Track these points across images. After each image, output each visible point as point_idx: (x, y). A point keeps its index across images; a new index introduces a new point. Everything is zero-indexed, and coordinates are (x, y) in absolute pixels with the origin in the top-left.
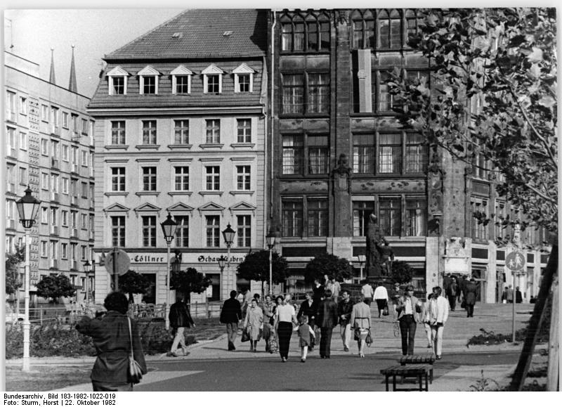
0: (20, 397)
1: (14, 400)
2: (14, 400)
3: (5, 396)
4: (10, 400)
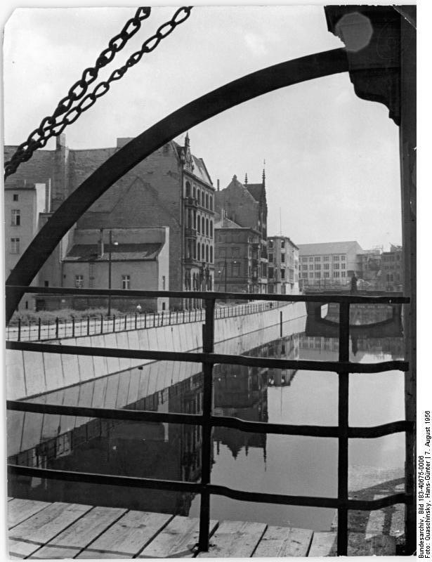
0: (422, 542)
1: (425, 549)
2: (425, 549)
3: (421, 557)
4: (425, 552)
